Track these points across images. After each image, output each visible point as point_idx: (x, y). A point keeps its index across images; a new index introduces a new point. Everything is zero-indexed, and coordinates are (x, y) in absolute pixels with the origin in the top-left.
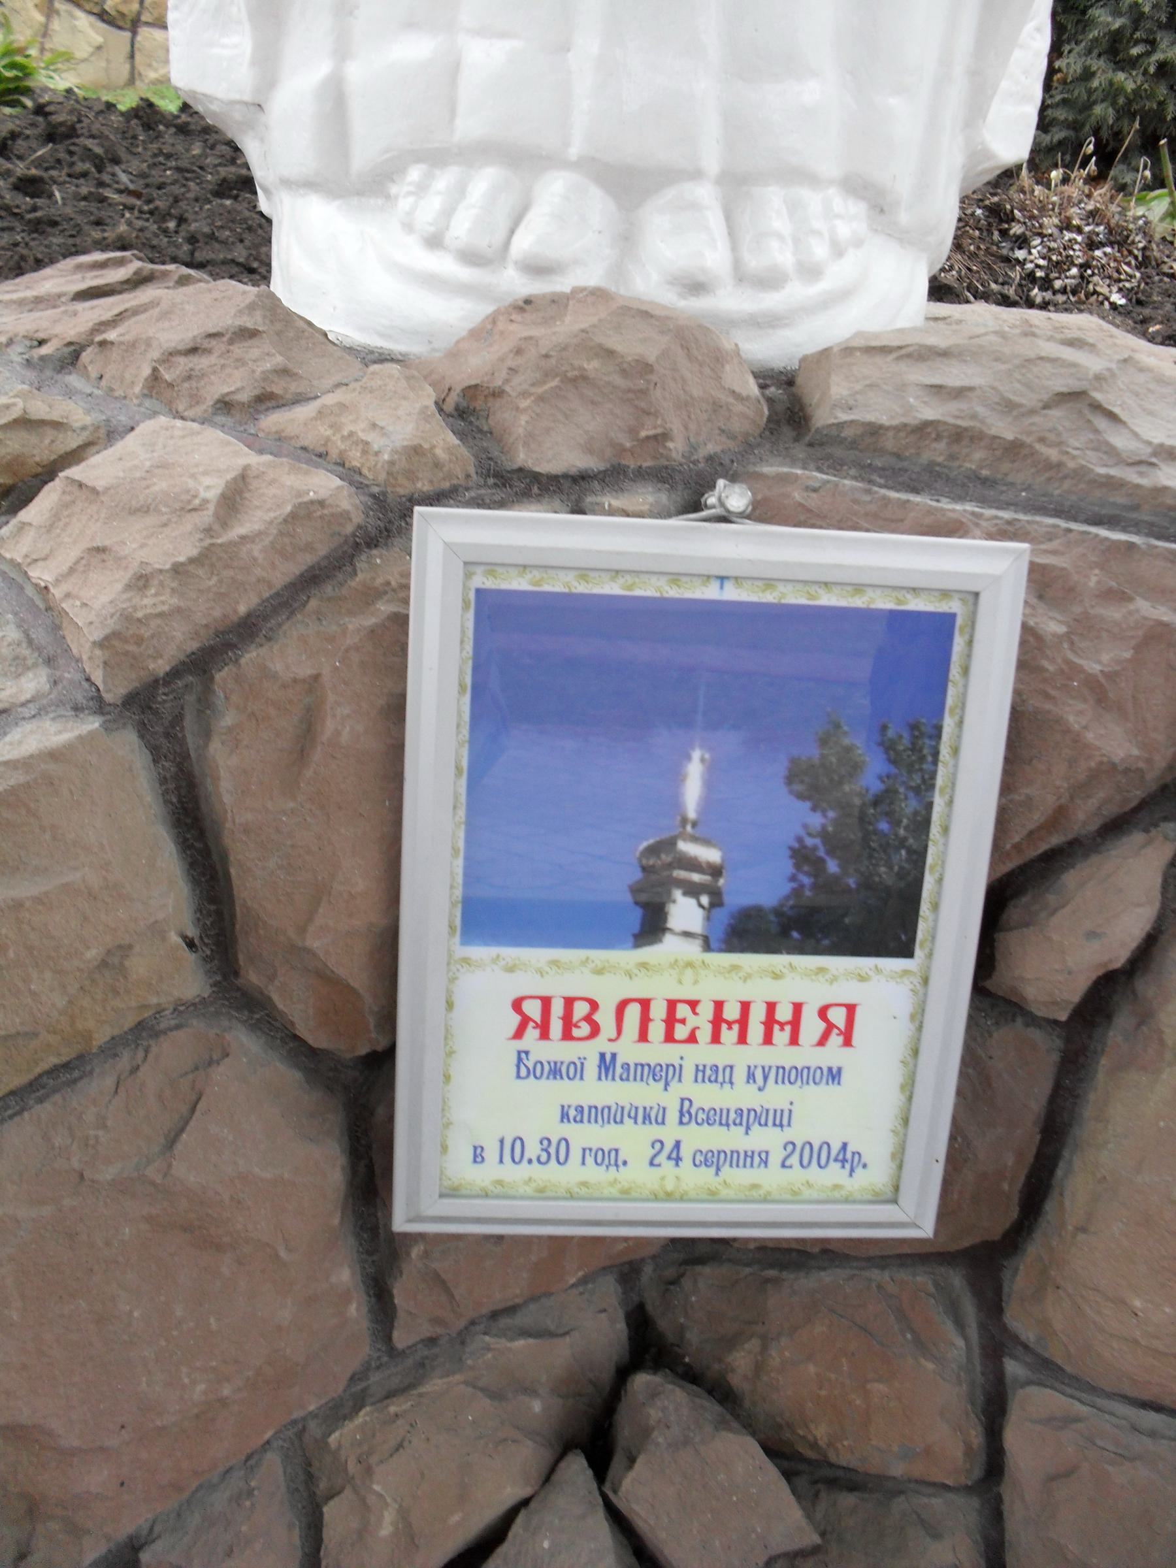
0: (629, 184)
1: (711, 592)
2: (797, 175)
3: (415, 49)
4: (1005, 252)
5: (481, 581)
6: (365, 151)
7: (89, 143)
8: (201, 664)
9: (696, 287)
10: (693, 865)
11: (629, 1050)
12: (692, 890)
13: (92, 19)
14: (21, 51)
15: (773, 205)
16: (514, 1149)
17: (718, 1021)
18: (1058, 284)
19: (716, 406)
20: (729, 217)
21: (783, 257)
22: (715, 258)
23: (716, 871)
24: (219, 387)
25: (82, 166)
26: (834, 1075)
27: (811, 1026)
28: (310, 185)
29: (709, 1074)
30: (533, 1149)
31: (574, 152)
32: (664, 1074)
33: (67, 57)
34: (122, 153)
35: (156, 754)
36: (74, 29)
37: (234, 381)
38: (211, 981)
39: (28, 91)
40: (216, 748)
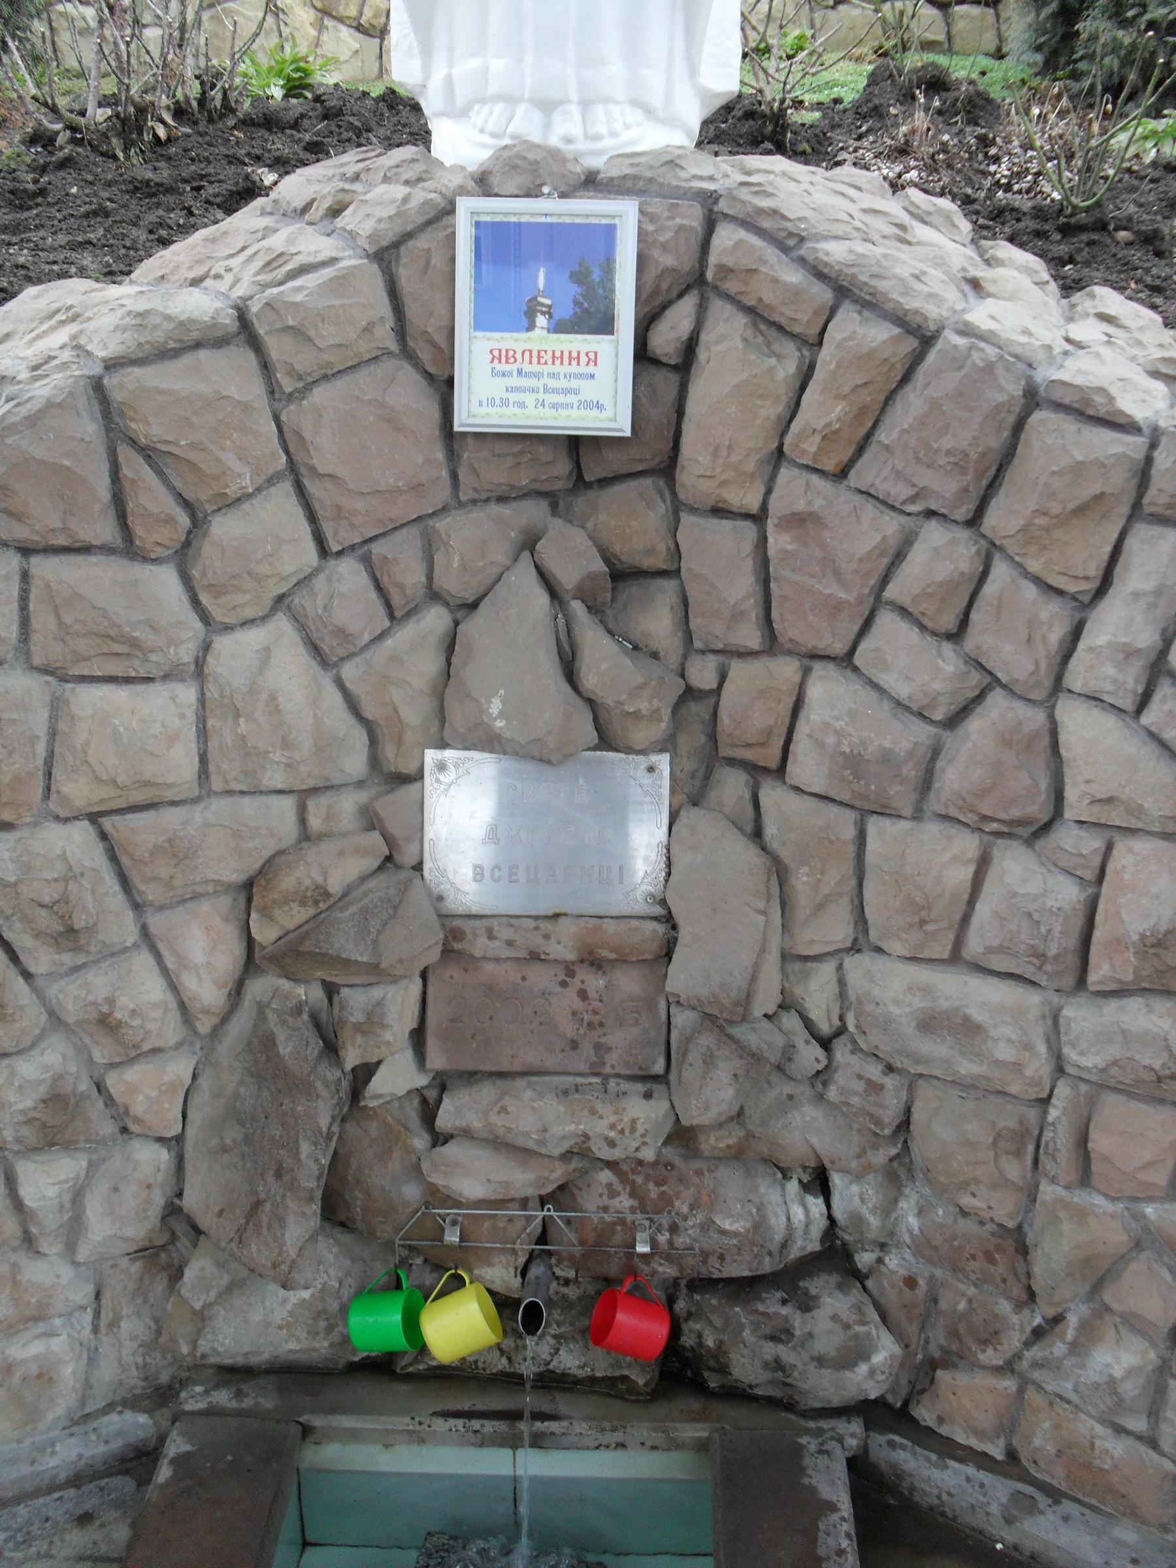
0: (547, 107)
1: (543, 220)
2: (607, 100)
3: (474, 63)
4: (982, 167)
5: (476, 218)
6: (460, 102)
7: (351, 119)
8: (396, 245)
9: (569, 141)
10: (542, 305)
11: (526, 367)
12: (543, 313)
13: (352, 31)
14: (304, 59)
15: (599, 111)
16: (491, 402)
17: (554, 357)
18: (1016, 187)
19: (564, 176)
20: (583, 115)
21: (604, 130)
22: (577, 131)
23: (550, 307)
24: (405, 177)
25: (345, 135)
26: (592, 376)
27: (583, 359)
28: (442, 114)
29: (553, 376)
30: (498, 402)
31: (526, 96)
32: (537, 375)
33: (336, 61)
34: (373, 125)
35: (383, 272)
36: (338, 39)
37: (410, 174)
38: (525, 1484)
39: (308, 87)
40: (401, 270)
